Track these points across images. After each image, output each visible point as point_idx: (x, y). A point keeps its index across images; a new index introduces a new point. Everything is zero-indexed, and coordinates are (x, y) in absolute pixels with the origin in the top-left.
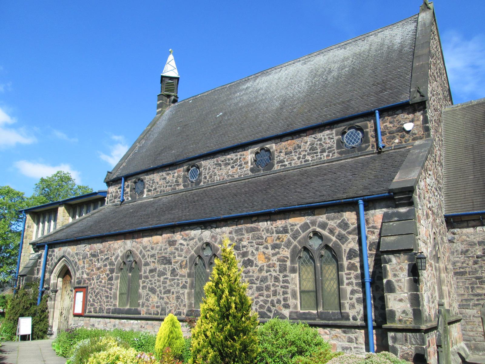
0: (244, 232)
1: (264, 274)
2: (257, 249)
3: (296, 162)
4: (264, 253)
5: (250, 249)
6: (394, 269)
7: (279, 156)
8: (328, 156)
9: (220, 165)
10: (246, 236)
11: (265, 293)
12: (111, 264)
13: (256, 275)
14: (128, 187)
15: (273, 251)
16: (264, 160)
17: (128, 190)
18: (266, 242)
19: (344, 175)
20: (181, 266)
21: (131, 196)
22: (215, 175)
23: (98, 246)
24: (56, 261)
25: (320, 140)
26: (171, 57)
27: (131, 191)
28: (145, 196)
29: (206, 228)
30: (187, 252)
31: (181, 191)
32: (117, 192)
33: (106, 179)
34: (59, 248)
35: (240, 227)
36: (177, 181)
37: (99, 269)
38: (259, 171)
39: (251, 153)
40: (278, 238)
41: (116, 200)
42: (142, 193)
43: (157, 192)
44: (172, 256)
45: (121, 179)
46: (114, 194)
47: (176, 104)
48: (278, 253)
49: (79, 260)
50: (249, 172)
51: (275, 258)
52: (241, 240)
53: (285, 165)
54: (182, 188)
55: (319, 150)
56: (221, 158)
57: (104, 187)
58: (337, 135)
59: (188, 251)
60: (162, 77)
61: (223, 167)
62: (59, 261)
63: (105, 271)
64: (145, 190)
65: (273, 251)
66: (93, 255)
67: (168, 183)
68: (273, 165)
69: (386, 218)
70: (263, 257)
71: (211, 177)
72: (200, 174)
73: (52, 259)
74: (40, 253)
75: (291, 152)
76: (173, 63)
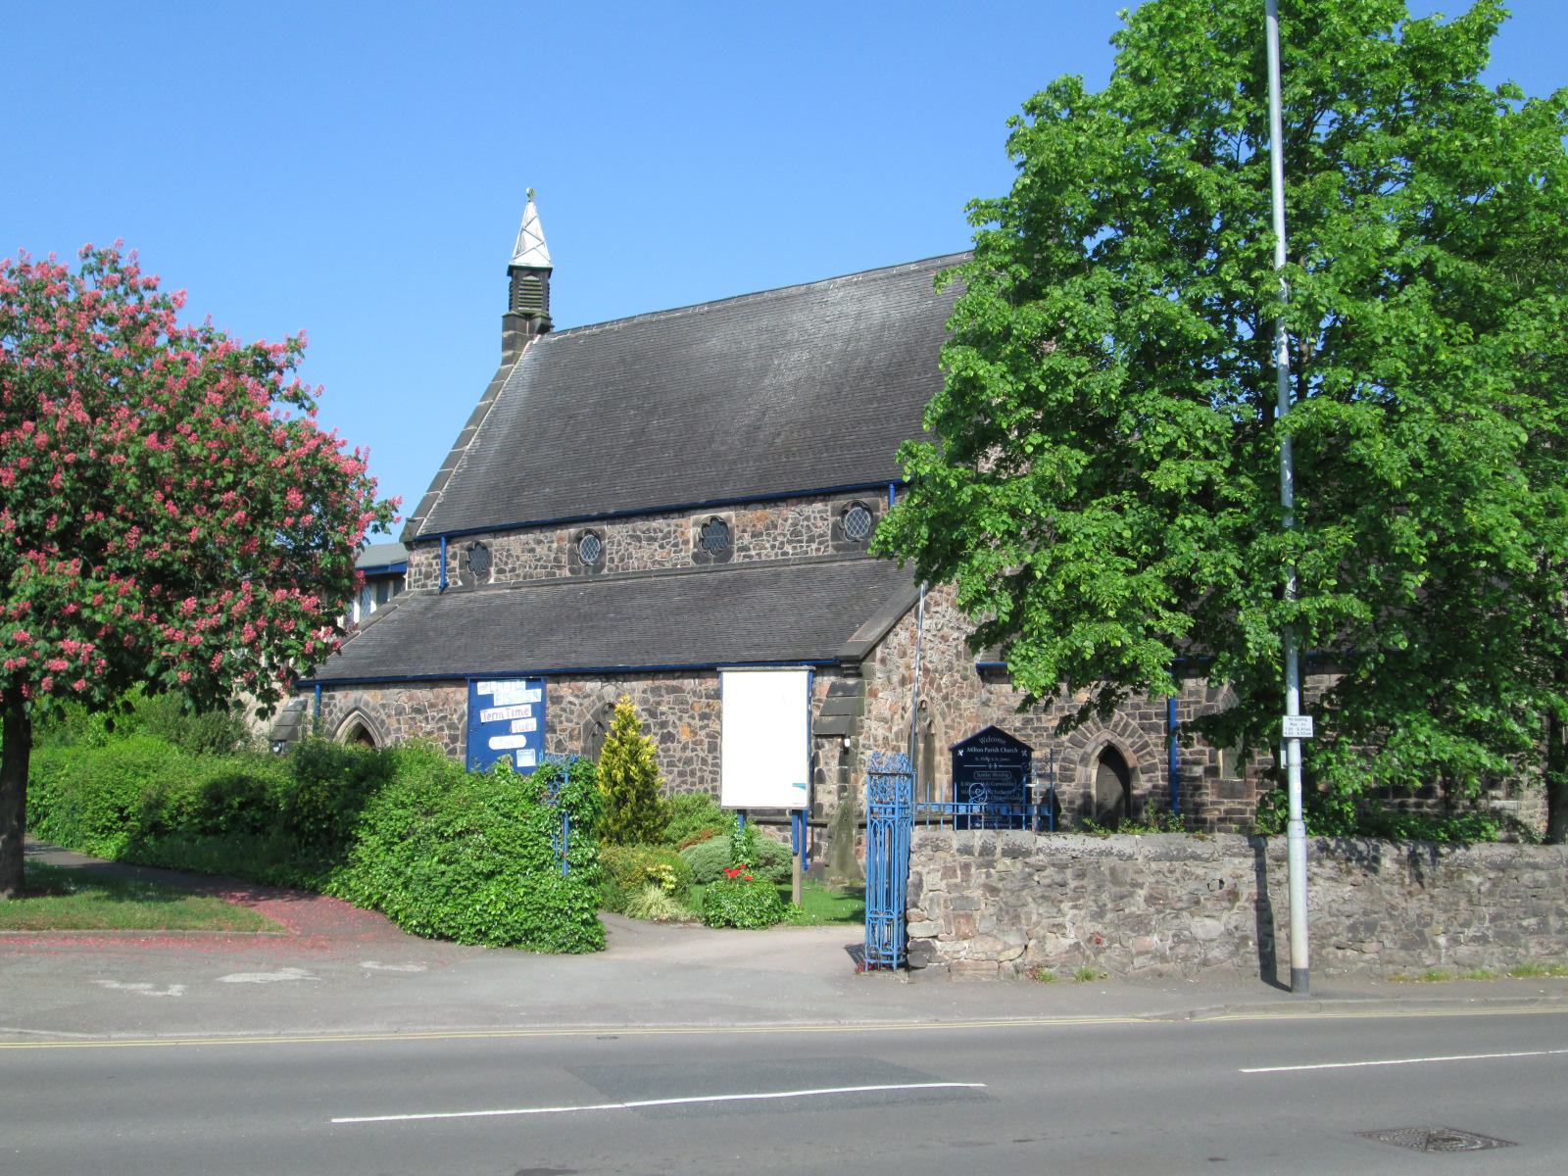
0: (663, 692)
1: (688, 753)
2: (680, 719)
3: (769, 553)
4: (689, 725)
5: (671, 718)
6: (826, 757)
7: (741, 538)
8: (818, 550)
9: (639, 540)
10: (666, 698)
11: (689, 779)
12: (452, 726)
13: (678, 755)
14: (454, 556)
15: (701, 723)
16: (716, 540)
17: (455, 564)
18: (692, 708)
19: (443, 891)
20: (571, 737)
21: (462, 577)
22: (630, 557)
23: (424, 695)
24: (341, 716)
25: (808, 519)
26: (531, 209)
27: (461, 567)
28: (492, 581)
29: (608, 680)
30: (579, 716)
31: (566, 581)
32: (431, 565)
33: (403, 534)
34: (343, 693)
35: (657, 683)
36: (556, 559)
37: (430, 733)
38: (707, 560)
39: (695, 524)
40: (708, 705)
41: (429, 582)
42: (487, 574)
43: (518, 576)
44: (556, 721)
45: (439, 540)
46: (423, 569)
47: (547, 338)
48: (707, 726)
49: (389, 716)
50: (690, 560)
51: (703, 733)
52: (658, 704)
53: (750, 557)
54: (568, 574)
55: (805, 538)
56: (641, 525)
57: (401, 553)
58: (833, 515)
59: (581, 715)
60: (512, 270)
61: (644, 543)
62: (347, 716)
63: (442, 738)
64: (493, 570)
65: (701, 723)
66: (418, 711)
67: (539, 560)
68: (730, 554)
69: (833, 689)
70: (688, 730)
71: (622, 560)
72: (602, 552)
73: (331, 713)
74: (302, 698)
75: (761, 534)
76: (536, 227)
